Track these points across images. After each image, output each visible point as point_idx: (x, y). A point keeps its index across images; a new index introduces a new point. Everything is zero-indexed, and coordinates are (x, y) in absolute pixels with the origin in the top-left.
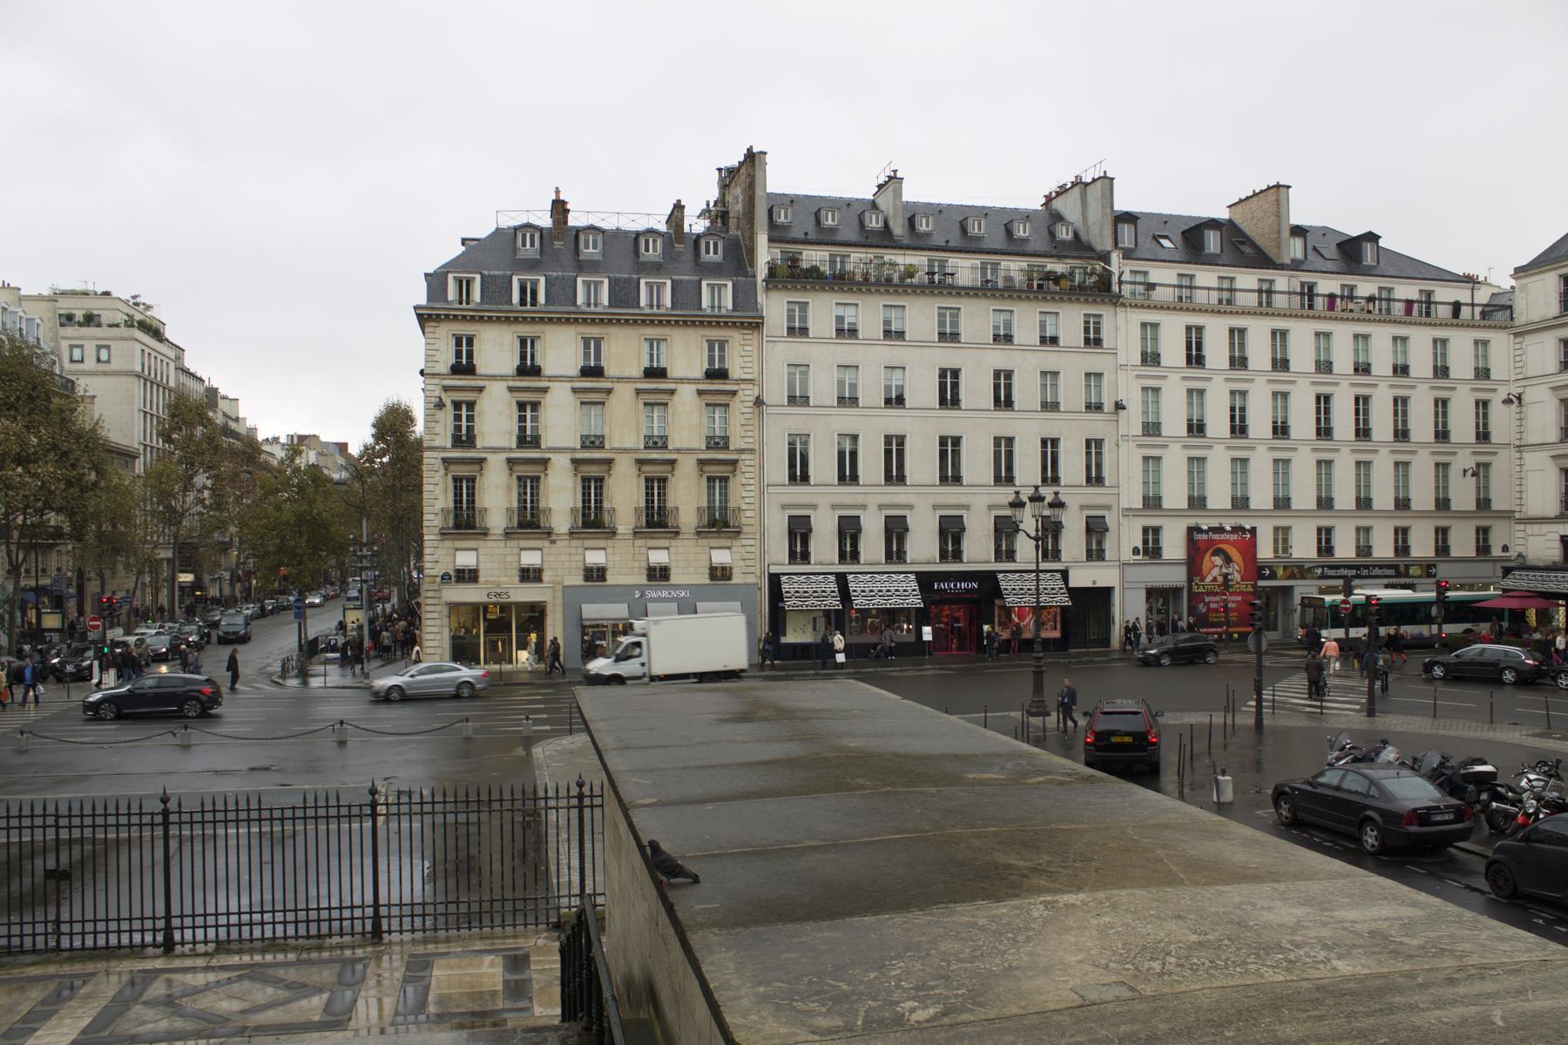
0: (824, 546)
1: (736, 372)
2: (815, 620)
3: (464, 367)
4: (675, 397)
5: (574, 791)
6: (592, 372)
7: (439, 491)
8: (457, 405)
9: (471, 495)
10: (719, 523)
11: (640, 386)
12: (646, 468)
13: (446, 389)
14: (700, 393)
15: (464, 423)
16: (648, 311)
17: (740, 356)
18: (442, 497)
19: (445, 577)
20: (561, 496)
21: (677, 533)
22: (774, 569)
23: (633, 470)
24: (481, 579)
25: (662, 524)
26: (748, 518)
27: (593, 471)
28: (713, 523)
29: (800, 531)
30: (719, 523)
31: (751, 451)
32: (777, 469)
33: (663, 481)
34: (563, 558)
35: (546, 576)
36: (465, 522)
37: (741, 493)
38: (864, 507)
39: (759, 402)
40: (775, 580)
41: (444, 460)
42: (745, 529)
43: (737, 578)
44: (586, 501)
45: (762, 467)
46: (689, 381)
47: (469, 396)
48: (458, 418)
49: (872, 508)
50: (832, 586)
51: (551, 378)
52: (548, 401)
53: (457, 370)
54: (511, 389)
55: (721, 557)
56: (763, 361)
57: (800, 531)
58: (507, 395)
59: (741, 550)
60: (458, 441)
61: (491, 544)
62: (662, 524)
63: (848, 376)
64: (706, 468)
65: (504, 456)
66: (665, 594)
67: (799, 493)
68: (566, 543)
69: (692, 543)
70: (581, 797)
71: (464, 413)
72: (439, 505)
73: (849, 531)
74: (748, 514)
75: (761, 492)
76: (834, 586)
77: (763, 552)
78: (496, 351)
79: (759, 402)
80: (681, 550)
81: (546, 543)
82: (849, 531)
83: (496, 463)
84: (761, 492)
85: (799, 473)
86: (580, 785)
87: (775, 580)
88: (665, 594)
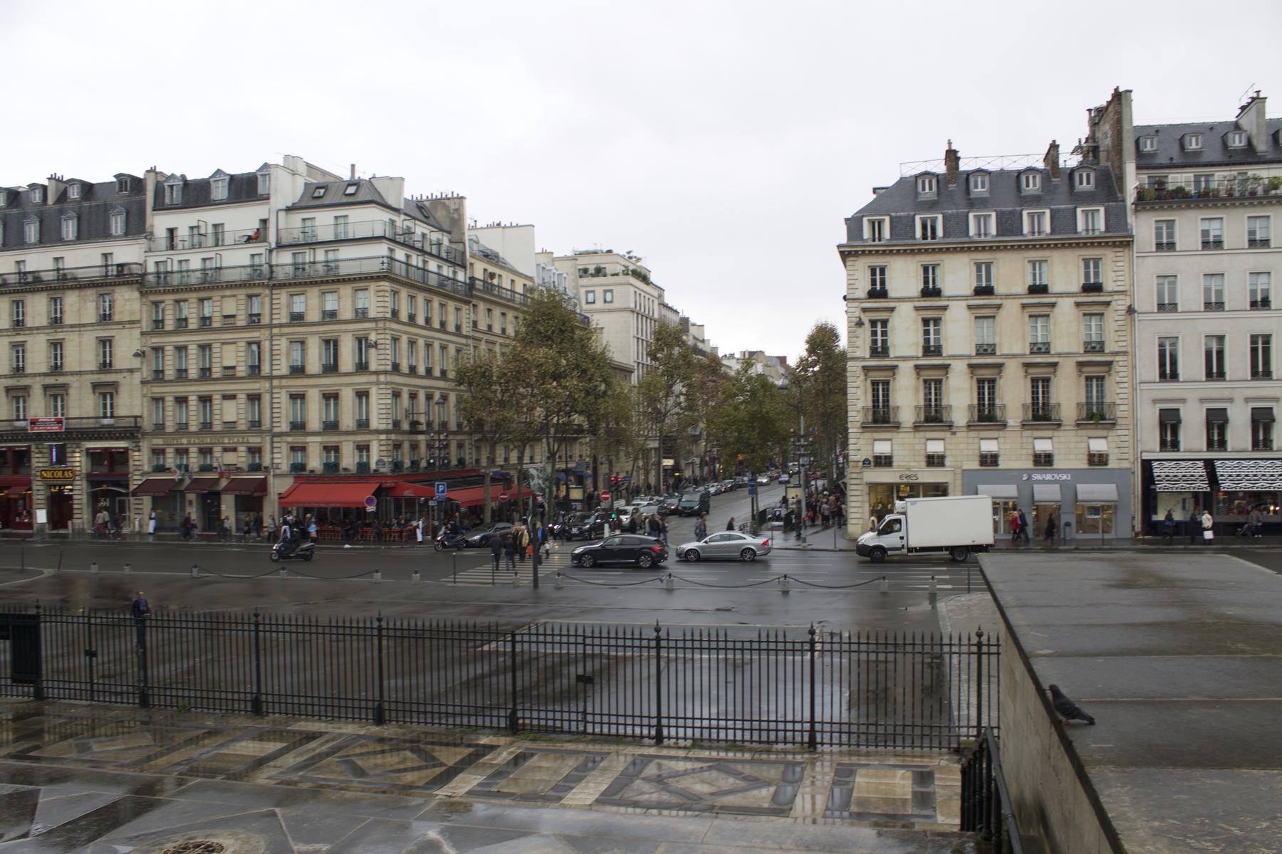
0: (1193, 435)
1: (1109, 285)
2: (1184, 500)
3: (878, 293)
4: (1056, 310)
5: (975, 640)
6: (984, 291)
7: (860, 392)
8: (873, 323)
9: (886, 395)
10: (1096, 416)
11: (1025, 301)
12: (1031, 370)
13: (864, 310)
14: (1078, 305)
15: (879, 338)
16: (1030, 237)
17: (1112, 271)
18: (862, 398)
19: (866, 462)
20: (959, 395)
21: (1059, 425)
22: (1146, 456)
23: (1020, 372)
24: (895, 464)
25: (1046, 418)
26: (1122, 411)
27: (987, 374)
28: (1036, 417)
29: (1170, 423)
30: (1096, 416)
31: (1125, 353)
32: (1148, 367)
33: (1046, 381)
34: (962, 446)
35: (948, 462)
36: (882, 417)
37: (1116, 390)
38: (1231, 400)
39: (1131, 310)
40: (1147, 466)
41: (864, 368)
42: (1120, 421)
43: (1112, 464)
44: (1089, 396)
45: (1134, 367)
46: (910, 299)
47: (882, 316)
48: (874, 333)
49: (1239, 402)
50: (1200, 470)
51: (950, 298)
52: (948, 317)
53: (873, 294)
54: (917, 309)
55: (1098, 446)
56: (1134, 274)
57: (1170, 423)
58: (914, 314)
59: (1117, 439)
60: (928, 350)
61: (902, 435)
62: (1046, 418)
63: (1214, 284)
64: (1085, 369)
65: (912, 363)
66: (1049, 477)
67: (1169, 390)
68: (964, 434)
69: (1073, 433)
70: (979, 645)
71: (879, 329)
72: (860, 404)
73: (1217, 422)
74: (1122, 408)
75: (1134, 389)
76: (1202, 471)
77: (1136, 441)
78: (904, 277)
79: (1131, 310)
80: (1062, 440)
81: (948, 435)
82: (1217, 422)
83: (906, 370)
84: (1134, 389)
85: (1169, 371)
86: (980, 635)
87: (1147, 466)
88: (1049, 477)
